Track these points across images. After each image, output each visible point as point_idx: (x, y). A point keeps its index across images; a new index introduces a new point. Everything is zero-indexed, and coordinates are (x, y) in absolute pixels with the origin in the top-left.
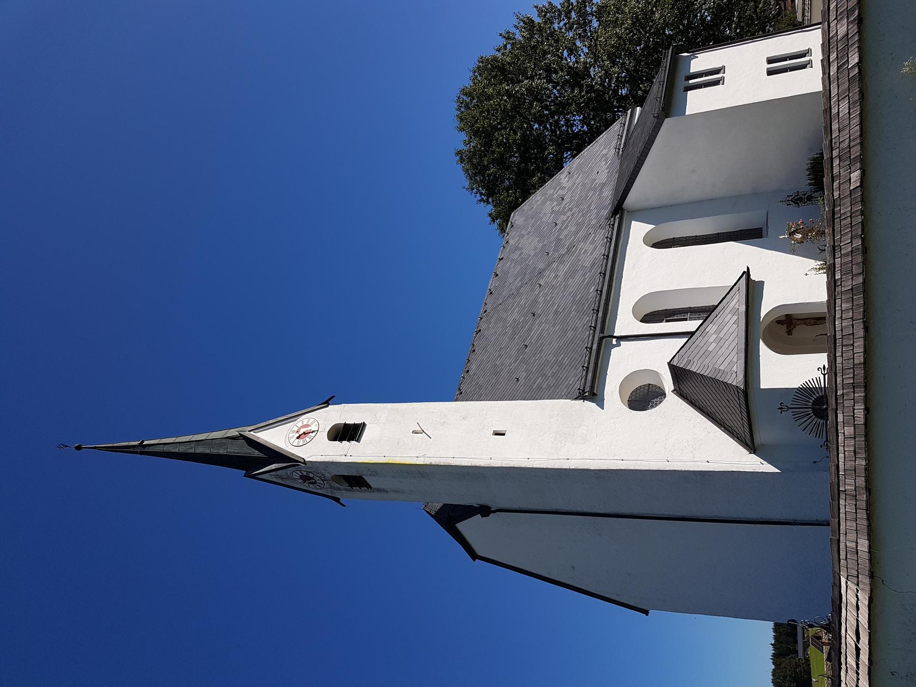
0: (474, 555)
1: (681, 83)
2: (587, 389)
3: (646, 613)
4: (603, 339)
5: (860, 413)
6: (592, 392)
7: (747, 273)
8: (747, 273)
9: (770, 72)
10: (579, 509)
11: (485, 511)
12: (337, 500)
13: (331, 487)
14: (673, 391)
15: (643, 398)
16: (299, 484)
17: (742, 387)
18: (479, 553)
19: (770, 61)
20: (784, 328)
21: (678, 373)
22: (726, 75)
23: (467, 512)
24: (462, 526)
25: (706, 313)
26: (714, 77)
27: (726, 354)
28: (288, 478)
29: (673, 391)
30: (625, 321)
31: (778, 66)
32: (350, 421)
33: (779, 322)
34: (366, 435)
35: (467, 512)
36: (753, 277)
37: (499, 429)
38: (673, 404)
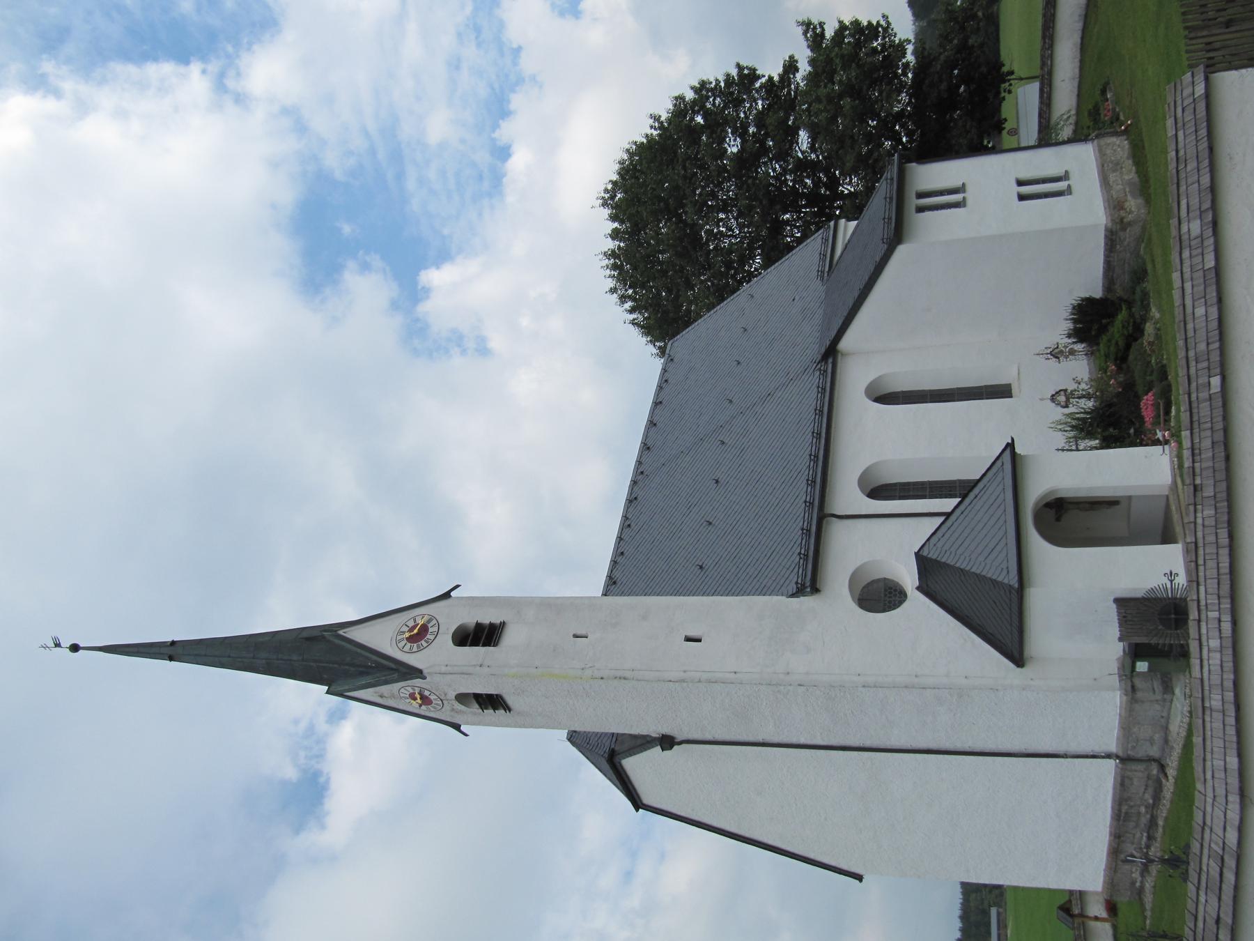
0: (637, 804)
1: (912, 202)
2: (808, 584)
3: (859, 878)
4: (819, 517)
5: (1227, 627)
6: (810, 585)
7: (1010, 446)
8: (1010, 446)
9: (1022, 198)
10: (794, 740)
11: (667, 742)
12: (457, 727)
13: (453, 710)
14: (918, 588)
15: (879, 596)
16: (414, 706)
17: (1016, 586)
18: (647, 800)
19: (1068, 191)
20: (1051, 514)
21: (926, 565)
22: (970, 195)
23: (641, 743)
24: (631, 764)
25: (962, 489)
26: (954, 198)
27: (991, 546)
28: (393, 696)
29: (918, 588)
30: (847, 495)
31: (1031, 190)
32: (486, 620)
33: (1048, 505)
34: (510, 638)
35: (641, 743)
36: (1018, 450)
37: (693, 633)
38: (918, 605)
